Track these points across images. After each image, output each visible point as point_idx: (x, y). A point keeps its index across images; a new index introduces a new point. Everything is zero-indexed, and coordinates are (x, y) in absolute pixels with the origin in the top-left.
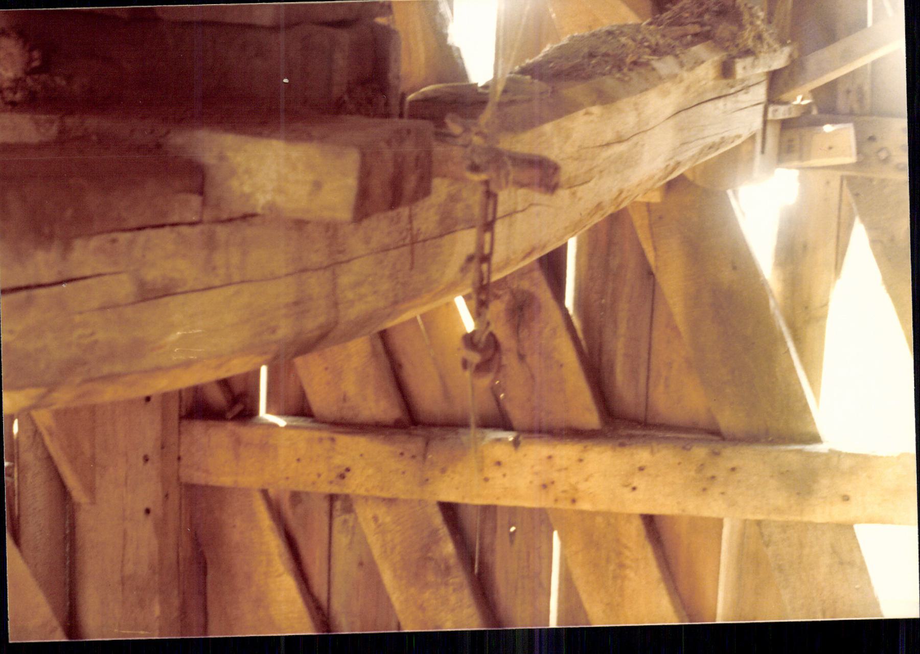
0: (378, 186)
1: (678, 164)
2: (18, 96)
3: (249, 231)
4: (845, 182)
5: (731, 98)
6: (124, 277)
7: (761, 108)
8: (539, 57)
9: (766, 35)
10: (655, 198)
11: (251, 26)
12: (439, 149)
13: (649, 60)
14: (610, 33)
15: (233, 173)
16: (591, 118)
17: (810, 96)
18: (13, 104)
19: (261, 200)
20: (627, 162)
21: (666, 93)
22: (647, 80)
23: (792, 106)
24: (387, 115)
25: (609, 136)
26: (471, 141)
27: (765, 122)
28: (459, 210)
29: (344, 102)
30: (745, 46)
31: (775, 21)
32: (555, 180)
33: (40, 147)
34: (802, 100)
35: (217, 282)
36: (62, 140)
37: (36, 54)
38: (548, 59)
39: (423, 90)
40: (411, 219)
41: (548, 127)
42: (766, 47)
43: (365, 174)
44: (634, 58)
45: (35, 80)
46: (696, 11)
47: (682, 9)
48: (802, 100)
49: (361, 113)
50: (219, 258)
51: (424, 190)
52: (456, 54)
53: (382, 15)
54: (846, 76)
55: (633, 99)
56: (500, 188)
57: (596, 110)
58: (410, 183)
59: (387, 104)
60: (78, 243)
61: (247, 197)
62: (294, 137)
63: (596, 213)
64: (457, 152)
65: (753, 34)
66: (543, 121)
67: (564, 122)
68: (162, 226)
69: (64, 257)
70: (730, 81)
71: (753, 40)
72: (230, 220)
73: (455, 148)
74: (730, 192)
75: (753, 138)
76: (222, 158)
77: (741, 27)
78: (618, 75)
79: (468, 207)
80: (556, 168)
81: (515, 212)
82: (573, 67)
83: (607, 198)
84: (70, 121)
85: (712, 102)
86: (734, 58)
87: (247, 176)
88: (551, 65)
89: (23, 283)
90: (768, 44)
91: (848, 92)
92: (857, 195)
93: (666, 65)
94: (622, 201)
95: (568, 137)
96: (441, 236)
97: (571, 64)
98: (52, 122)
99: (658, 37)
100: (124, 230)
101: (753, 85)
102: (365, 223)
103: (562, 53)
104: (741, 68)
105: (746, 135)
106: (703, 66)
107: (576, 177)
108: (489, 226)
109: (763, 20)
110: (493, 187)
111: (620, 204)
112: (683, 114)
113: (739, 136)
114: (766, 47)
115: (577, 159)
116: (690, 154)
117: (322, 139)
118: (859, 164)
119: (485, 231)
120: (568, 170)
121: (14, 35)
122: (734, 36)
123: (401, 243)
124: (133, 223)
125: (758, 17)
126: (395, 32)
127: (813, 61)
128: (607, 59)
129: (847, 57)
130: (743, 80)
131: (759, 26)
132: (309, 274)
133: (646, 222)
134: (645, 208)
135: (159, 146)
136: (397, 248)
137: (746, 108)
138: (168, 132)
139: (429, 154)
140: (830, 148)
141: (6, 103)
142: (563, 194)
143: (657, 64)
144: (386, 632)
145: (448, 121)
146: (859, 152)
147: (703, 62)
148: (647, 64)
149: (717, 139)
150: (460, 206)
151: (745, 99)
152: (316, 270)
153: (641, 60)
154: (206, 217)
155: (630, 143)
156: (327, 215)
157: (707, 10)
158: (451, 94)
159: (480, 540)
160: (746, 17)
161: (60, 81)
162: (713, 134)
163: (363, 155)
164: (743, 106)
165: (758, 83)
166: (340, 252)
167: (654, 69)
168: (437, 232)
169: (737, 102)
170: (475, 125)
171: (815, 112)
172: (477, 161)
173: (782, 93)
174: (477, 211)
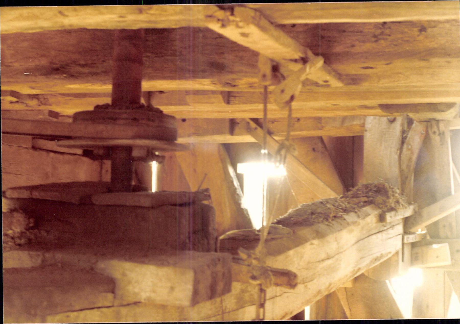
0: (203, 288)
1: (359, 269)
2: (22, 241)
4: (446, 274)
5: (385, 232)
7: (400, 237)
8: (286, 215)
9: (401, 201)
10: (349, 285)
12: (235, 267)
13: (342, 215)
14: (322, 203)
16: (314, 246)
17: (426, 229)
18: (20, 245)
19: (143, 296)
20: (332, 269)
21: (351, 231)
22: (341, 224)
23: (416, 235)
24: (208, 250)
25: (323, 256)
26: (252, 263)
27: (403, 244)
28: (247, 296)
30: (390, 206)
31: (405, 194)
32: (295, 282)
34: (422, 231)
36: (43, 267)
37: (32, 220)
38: (290, 216)
39: (228, 233)
40: (221, 301)
41: (291, 252)
42: (401, 206)
43: (196, 282)
44: (334, 215)
45: (31, 233)
46: (365, 190)
47: (358, 190)
48: (422, 231)
51: (227, 289)
52: (245, 213)
53: (205, 200)
54: (443, 219)
55: (335, 235)
56: (267, 287)
57: (316, 242)
58: (220, 286)
59: (208, 244)
61: (136, 294)
62: (161, 264)
63: (318, 295)
64: (244, 269)
65: (394, 200)
66: (289, 249)
67: (299, 249)
70: (384, 223)
71: (395, 204)
72: (128, 305)
73: (244, 266)
74: (387, 281)
75: (397, 253)
76: (124, 275)
77: (388, 197)
78: (327, 223)
79: (251, 295)
80: (295, 276)
81: (276, 296)
82: (303, 220)
83: (323, 288)
84: (47, 255)
85: (375, 235)
86: (385, 212)
88: (292, 219)
90: (402, 205)
91: (444, 226)
92: (453, 280)
93: (350, 217)
94: (332, 289)
95: (302, 257)
96: (238, 309)
97: (302, 218)
98: (38, 256)
99: (346, 204)
100: (74, 311)
101: (396, 225)
102: (197, 305)
103: (298, 213)
104: (389, 217)
105: (393, 252)
106: (370, 217)
107: (307, 278)
108: (262, 305)
109: (399, 194)
110: (263, 287)
111: (330, 291)
112: (361, 242)
113: (390, 253)
114: (401, 206)
115: (307, 269)
116: (365, 264)
117: (174, 265)
118: (453, 265)
119: (260, 308)
120: (301, 275)
121: (21, 211)
122: (385, 202)
123: (217, 314)
124: (78, 308)
125: (396, 193)
126: (212, 208)
127: (425, 211)
128: (320, 215)
129: (442, 209)
130: (390, 223)
131: (397, 197)
133: (345, 296)
134: (344, 290)
135: (92, 269)
136: (215, 316)
137: (393, 237)
138: (97, 261)
139: (230, 272)
140: (437, 257)
141: (16, 245)
142: (300, 287)
143: (345, 216)
145: (239, 252)
146: (452, 259)
147: (369, 215)
148: (341, 217)
149: (379, 255)
150: (247, 295)
151: (392, 232)
153: (338, 215)
155: (334, 259)
156: (177, 303)
157: (371, 190)
158: (243, 235)
159: (351, 116)
160: (390, 193)
161: (44, 233)
162: (376, 252)
163: (195, 272)
164: (391, 236)
165: (398, 224)
167: (345, 219)
168: (235, 308)
169: (388, 234)
170: (254, 254)
171: (428, 237)
172: (255, 274)
173: (411, 228)
174: (256, 296)
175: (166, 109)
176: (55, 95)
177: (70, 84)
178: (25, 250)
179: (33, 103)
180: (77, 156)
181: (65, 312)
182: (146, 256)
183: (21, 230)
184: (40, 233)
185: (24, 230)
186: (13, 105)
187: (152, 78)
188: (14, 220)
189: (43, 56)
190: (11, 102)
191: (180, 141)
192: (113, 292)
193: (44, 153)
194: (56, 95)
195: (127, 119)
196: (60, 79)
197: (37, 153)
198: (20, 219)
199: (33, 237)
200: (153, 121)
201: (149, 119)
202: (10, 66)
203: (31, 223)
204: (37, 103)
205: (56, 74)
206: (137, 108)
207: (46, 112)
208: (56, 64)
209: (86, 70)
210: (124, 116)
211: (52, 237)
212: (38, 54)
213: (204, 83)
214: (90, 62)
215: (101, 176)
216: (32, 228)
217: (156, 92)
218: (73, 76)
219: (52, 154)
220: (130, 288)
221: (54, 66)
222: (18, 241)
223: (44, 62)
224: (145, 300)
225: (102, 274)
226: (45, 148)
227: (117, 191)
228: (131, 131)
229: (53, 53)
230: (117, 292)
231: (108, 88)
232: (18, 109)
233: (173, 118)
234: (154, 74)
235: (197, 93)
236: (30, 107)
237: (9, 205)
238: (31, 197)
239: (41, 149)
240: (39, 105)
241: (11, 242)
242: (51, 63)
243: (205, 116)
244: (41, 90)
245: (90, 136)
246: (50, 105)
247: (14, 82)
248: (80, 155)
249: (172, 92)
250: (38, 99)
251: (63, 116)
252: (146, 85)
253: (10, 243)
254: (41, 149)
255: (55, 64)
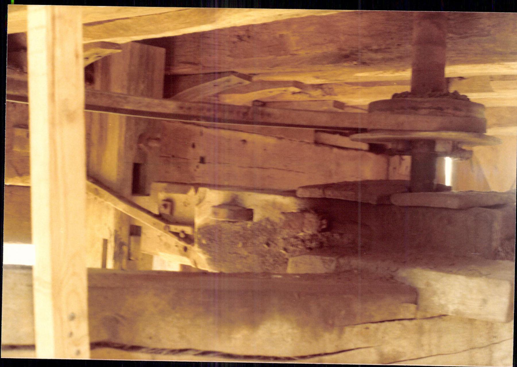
2: (313, 245)
3: (443, 324)
6: (372, 350)
11: (447, 209)
15: (434, 293)
18: (310, 249)
19: (451, 308)
29: (499, 251)
33: (327, 276)
35: (423, 355)
36: (338, 273)
37: (324, 222)
45: (323, 236)
49: (508, 259)
50: (425, 340)
60: (347, 329)
61: (442, 306)
62: (471, 274)
68: (394, 320)
69: (340, 337)
72: (432, 318)
76: (428, 284)
84: (342, 261)
87: (442, 295)
89: (317, 352)
98: (332, 261)
117: (487, 276)
124: (378, 319)
132: (476, 350)
135: (392, 277)
138: (397, 269)
144: (335, 364)
152: (480, 348)
154: (418, 316)
161: (337, 236)
166: (495, 337)
175: (473, 97)
176: (341, 85)
177: (359, 72)
178: (318, 255)
179: (317, 93)
180: (363, 152)
181: (365, 323)
182: (453, 265)
183: (313, 232)
184: (333, 236)
185: (316, 232)
186: (295, 96)
187: (454, 63)
188: (306, 221)
189: (331, 41)
190: (294, 93)
191: (490, 132)
192: (415, 303)
193: (327, 148)
194: (341, 84)
195: (430, 108)
196: (350, 67)
197: (319, 149)
198: (311, 220)
199: (324, 240)
200: (460, 110)
201: (456, 109)
202: (296, 55)
203: (324, 225)
204: (320, 93)
205: (345, 61)
206: (440, 96)
207: (331, 103)
208: (346, 50)
209: (379, 56)
210: (427, 105)
211: (345, 240)
212: (325, 39)
213: (512, 67)
214: (383, 47)
215: (388, 175)
216: (324, 230)
217: (455, 78)
218: (364, 63)
219: (335, 150)
220: (435, 299)
221: (344, 53)
222: (309, 244)
223: (332, 49)
224: (452, 313)
225: (403, 283)
226: (327, 142)
227: (419, 191)
228: (437, 121)
229: (343, 38)
230: (419, 302)
231: (407, 74)
232: (301, 100)
233: (481, 106)
234: (457, 58)
235: (504, 78)
236: (313, 97)
237: (299, 205)
238: (323, 197)
239: (323, 144)
240: (324, 96)
241: (301, 245)
242: (340, 49)
243: (509, 104)
244: (327, 79)
245: (390, 128)
246: (336, 95)
247: (298, 72)
248: (366, 151)
249: (473, 78)
250: (322, 88)
251: (348, 106)
252: (450, 71)
253: (300, 247)
254: (323, 144)
255: (343, 50)
